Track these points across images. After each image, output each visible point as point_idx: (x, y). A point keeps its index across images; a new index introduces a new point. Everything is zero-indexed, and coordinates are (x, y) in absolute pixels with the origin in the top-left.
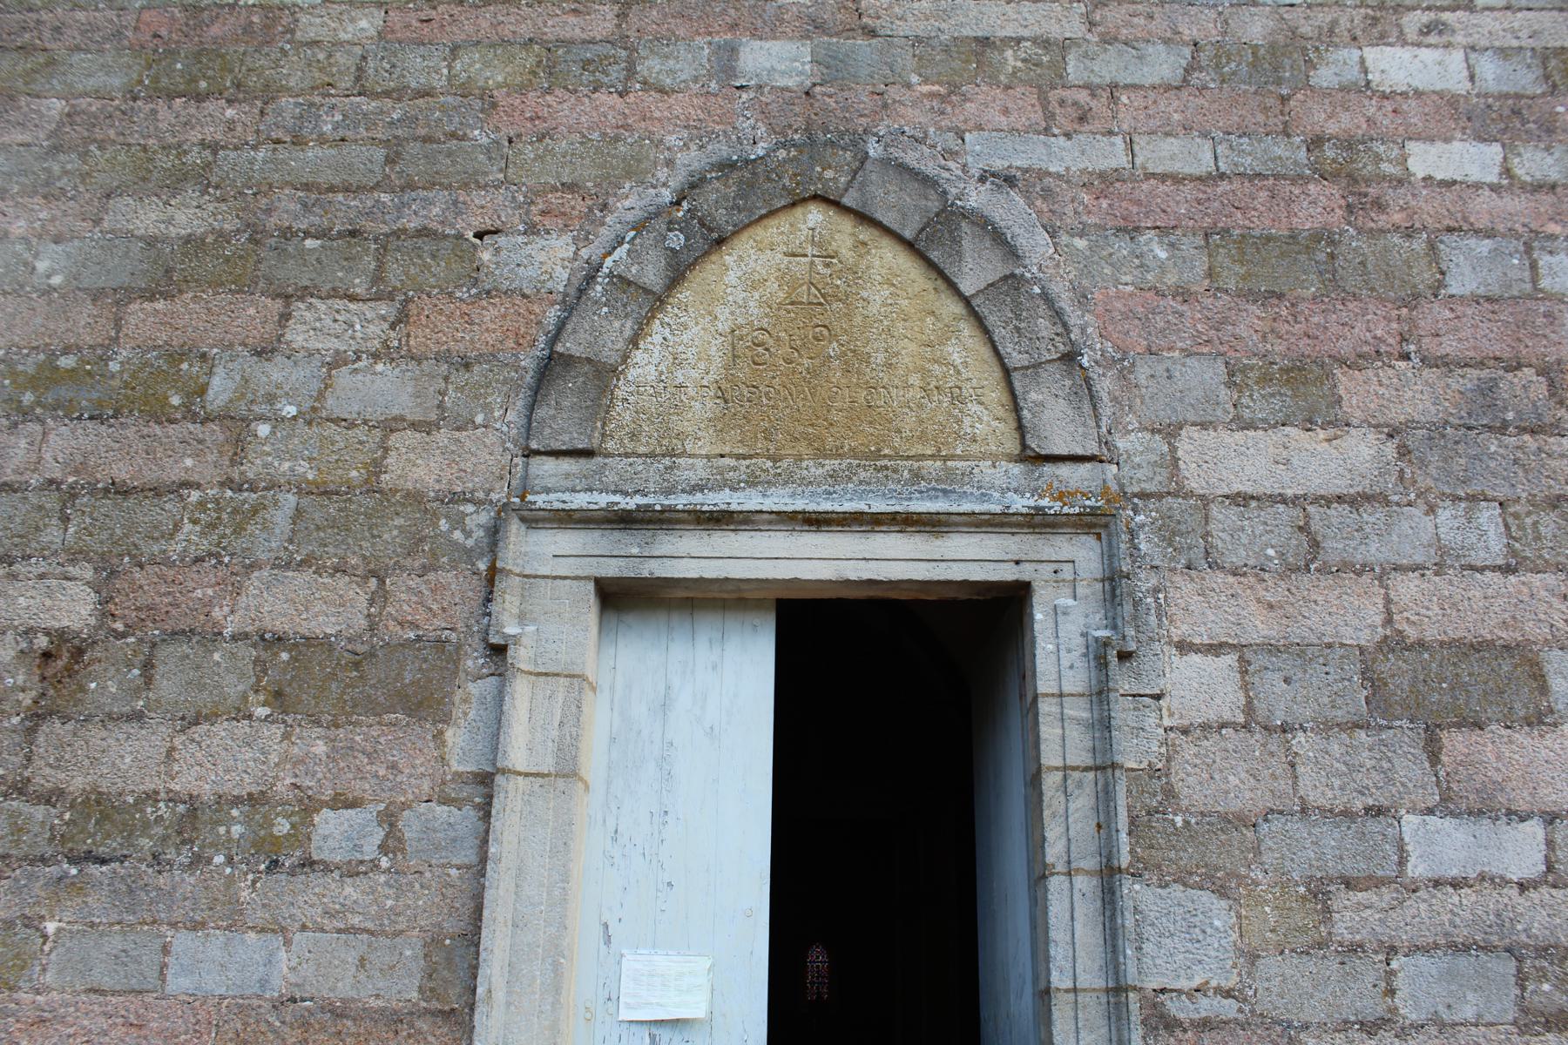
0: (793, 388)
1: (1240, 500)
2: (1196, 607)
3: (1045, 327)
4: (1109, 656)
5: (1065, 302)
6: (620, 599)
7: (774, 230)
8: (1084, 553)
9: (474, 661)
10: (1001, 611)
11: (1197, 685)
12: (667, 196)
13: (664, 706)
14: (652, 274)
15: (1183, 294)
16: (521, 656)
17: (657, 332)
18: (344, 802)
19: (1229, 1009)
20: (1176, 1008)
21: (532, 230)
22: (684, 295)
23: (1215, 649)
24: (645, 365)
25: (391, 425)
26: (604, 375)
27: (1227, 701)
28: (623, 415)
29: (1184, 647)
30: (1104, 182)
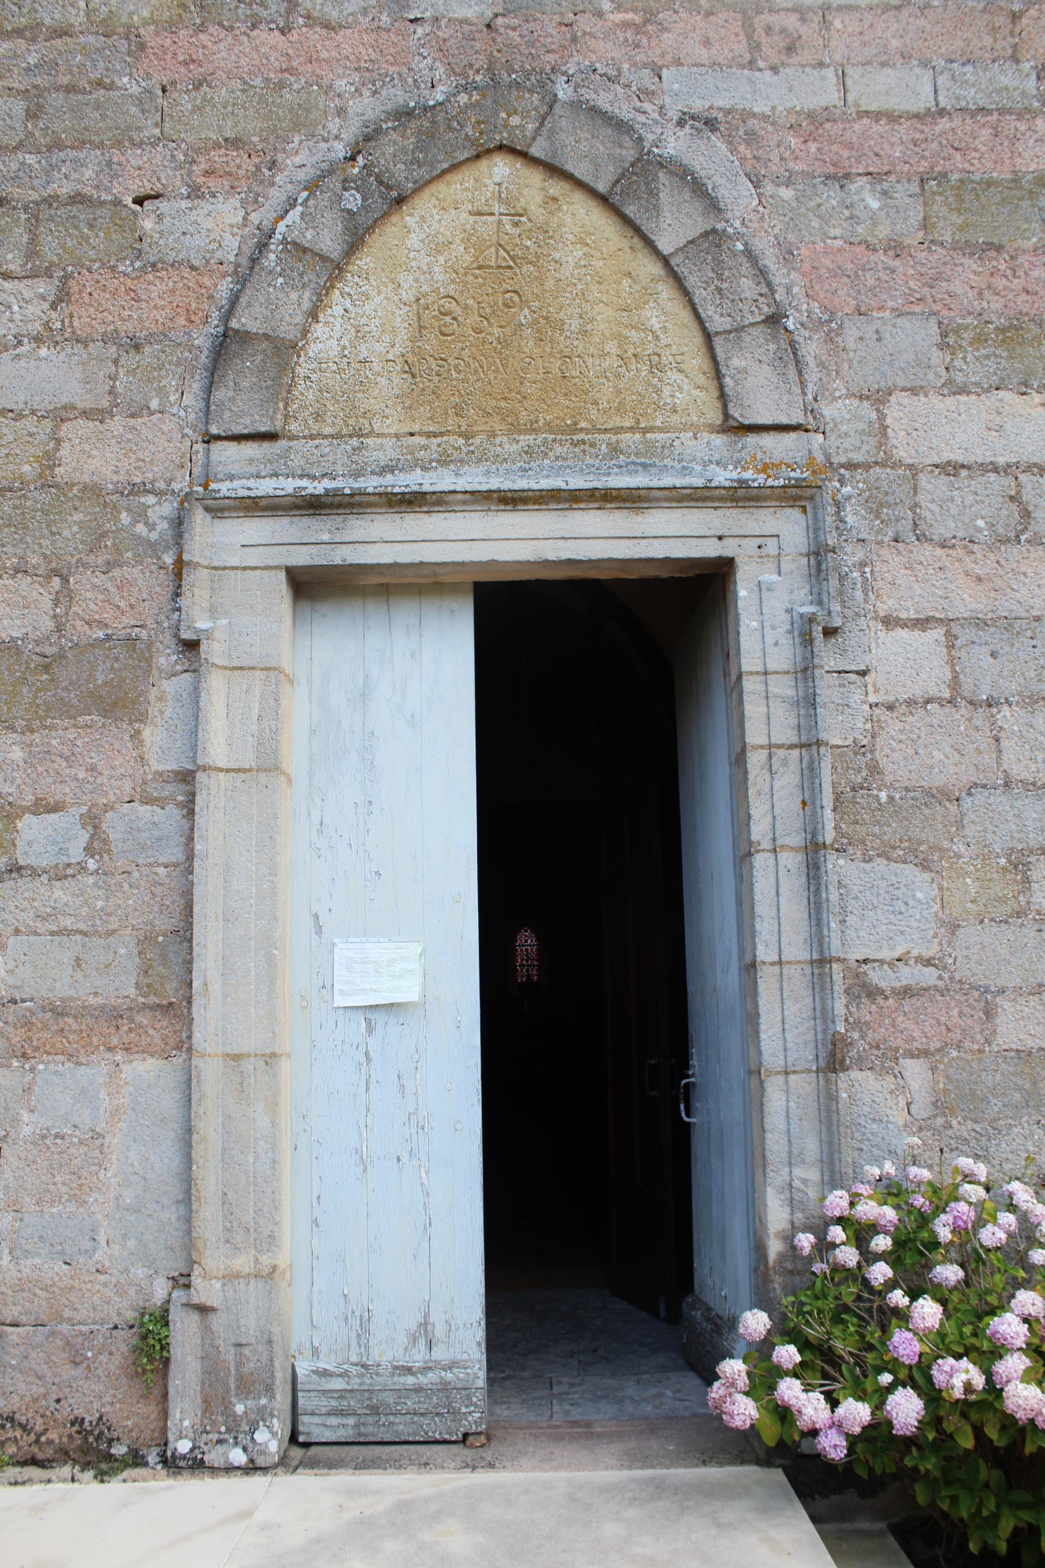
0: (484, 354)
1: (951, 469)
2: (905, 581)
3: (748, 287)
4: (815, 632)
5: (770, 260)
6: (309, 586)
7: (457, 187)
8: (789, 527)
9: (166, 657)
10: (703, 589)
11: (902, 661)
12: (340, 150)
13: (363, 696)
14: (328, 240)
15: (896, 248)
16: (213, 651)
17: (338, 303)
18: (45, 807)
19: (929, 976)
20: (877, 977)
21: (195, 193)
22: (364, 261)
23: (922, 623)
24: (326, 340)
25: (61, 415)
26: (284, 351)
27: (933, 677)
28: (305, 394)
29: (890, 622)
30: (813, 123)
